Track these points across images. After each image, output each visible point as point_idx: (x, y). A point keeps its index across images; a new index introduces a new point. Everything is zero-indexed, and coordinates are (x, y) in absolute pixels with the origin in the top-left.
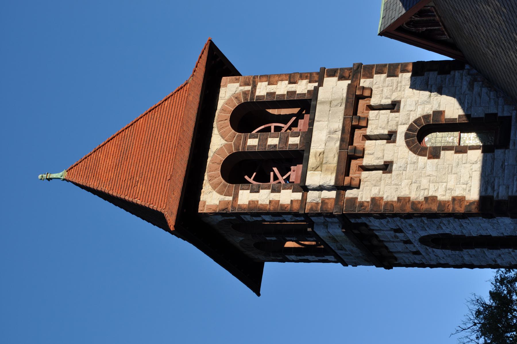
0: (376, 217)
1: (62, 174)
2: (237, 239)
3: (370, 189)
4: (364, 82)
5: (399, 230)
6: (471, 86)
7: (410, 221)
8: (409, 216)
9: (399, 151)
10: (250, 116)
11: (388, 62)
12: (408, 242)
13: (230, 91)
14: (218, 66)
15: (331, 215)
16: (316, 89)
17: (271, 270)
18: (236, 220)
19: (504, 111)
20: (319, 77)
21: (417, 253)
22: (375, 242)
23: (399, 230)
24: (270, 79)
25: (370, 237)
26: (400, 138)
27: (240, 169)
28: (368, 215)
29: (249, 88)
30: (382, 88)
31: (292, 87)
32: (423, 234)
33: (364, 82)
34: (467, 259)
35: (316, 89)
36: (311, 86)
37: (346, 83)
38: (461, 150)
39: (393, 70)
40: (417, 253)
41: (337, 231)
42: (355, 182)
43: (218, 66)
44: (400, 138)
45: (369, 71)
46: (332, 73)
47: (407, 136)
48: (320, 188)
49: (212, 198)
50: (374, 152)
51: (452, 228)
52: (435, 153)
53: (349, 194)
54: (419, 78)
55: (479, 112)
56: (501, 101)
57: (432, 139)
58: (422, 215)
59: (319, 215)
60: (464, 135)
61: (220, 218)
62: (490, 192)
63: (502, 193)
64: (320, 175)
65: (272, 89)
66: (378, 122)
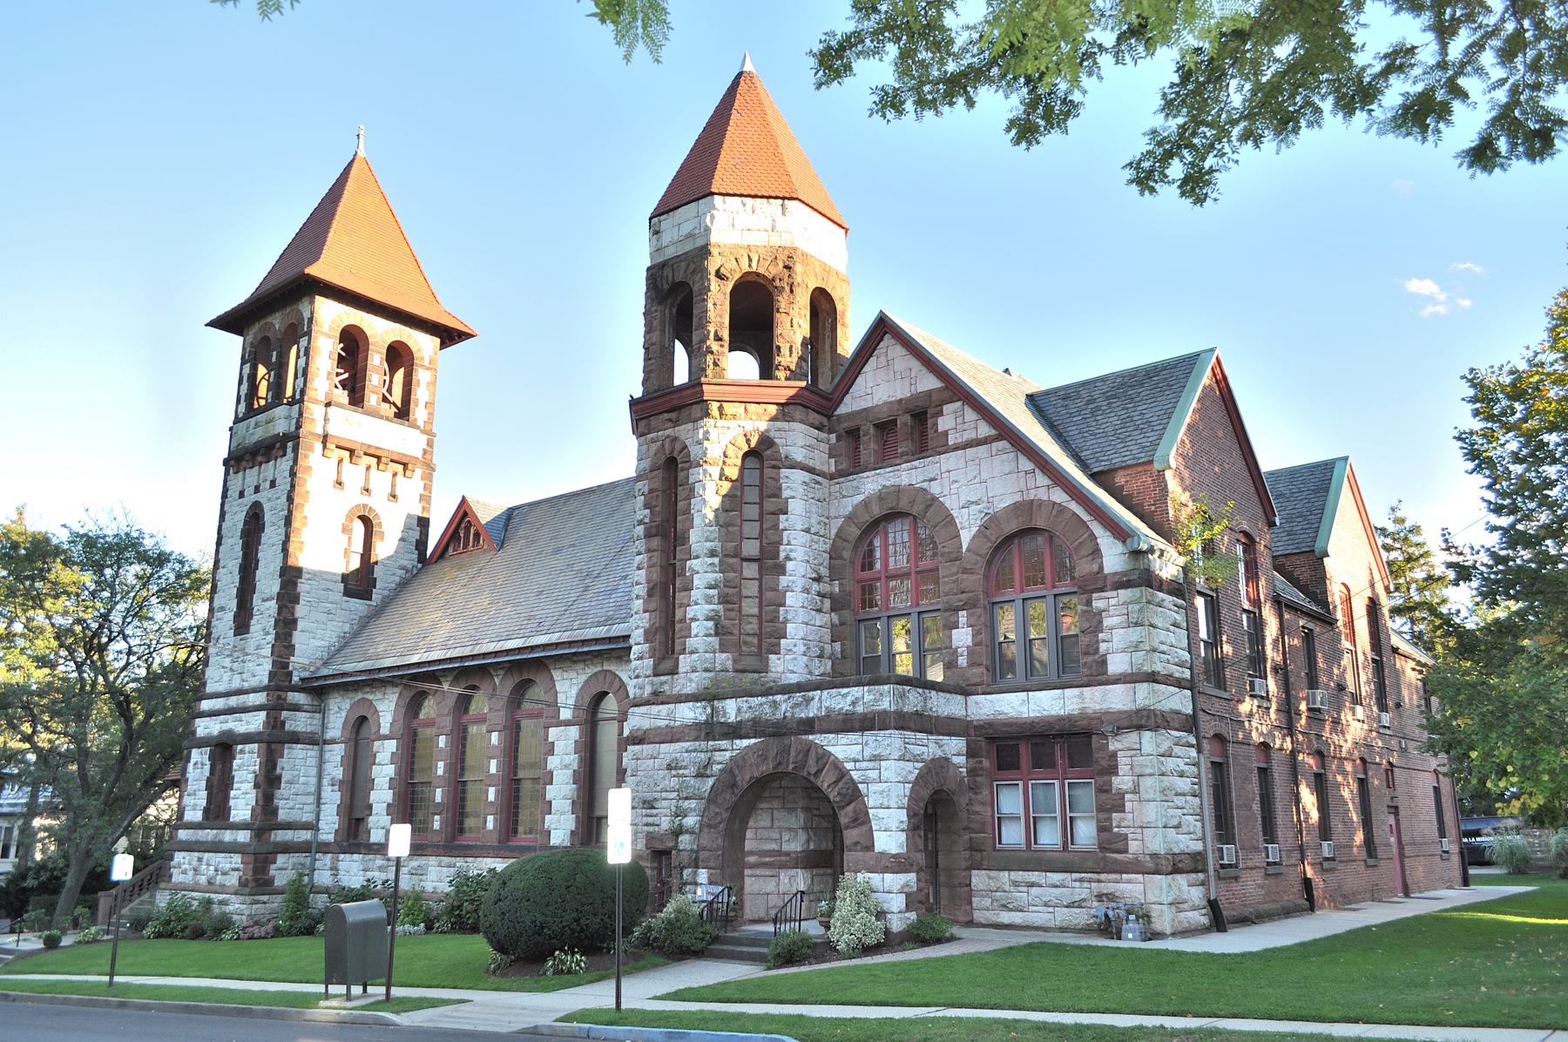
0: (292, 468)
1: (362, 154)
2: (277, 321)
3: (318, 467)
4: (419, 472)
5: (273, 484)
6: (403, 568)
7: (284, 498)
8: (290, 499)
9: (352, 497)
10: (398, 356)
11: (433, 495)
12: (257, 489)
13: (422, 344)
14: (449, 336)
15: (298, 427)
16: (418, 427)
17: (232, 345)
18: (299, 331)
19: (377, 595)
20: (429, 433)
21: (242, 495)
22: (260, 458)
23: (273, 484)
24: (433, 383)
25: (262, 450)
26: (364, 500)
27: (353, 344)
28: (295, 461)
29: (426, 363)
30: (410, 487)
31: (422, 404)
32: (266, 507)
33: (419, 472)
34: (227, 542)
35: (418, 427)
36: (420, 423)
37: (419, 455)
38: (347, 553)
39: (425, 499)
40: (242, 495)
41: (281, 427)
42: (328, 453)
43: (449, 336)
44: (364, 500)
45: (428, 477)
46: (430, 444)
47: (365, 506)
48: (326, 419)
49: (329, 316)
50: (354, 474)
51: (271, 536)
52: (346, 529)
53: (318, 446)
54: (415, 522)
55: (378, 572)
56: (386, 593)
57: (359, 527)
58: (290, 512)
59: (301, 414)
60: (358, 557)
61: (306, 315)
62: (305, 576)
63: (303, 587)
64: (348, 424)
65: (423, 384)
66: (381, 480)
